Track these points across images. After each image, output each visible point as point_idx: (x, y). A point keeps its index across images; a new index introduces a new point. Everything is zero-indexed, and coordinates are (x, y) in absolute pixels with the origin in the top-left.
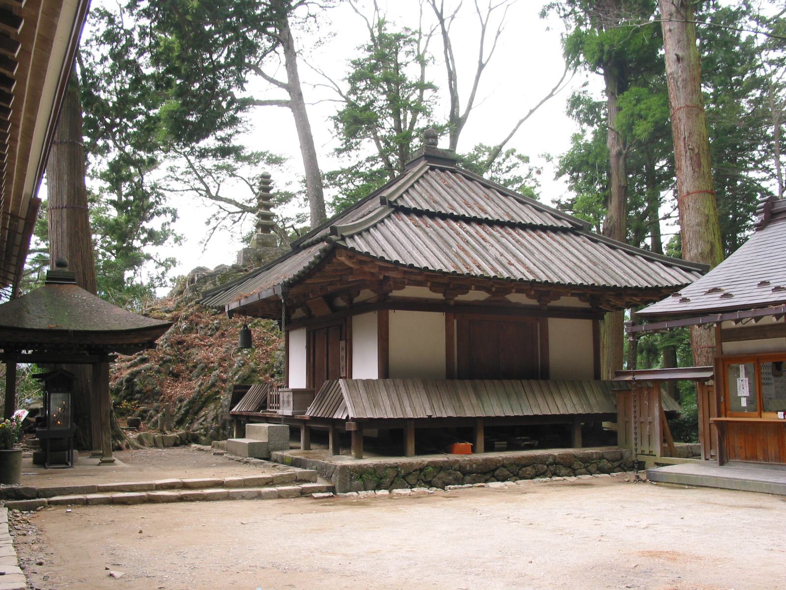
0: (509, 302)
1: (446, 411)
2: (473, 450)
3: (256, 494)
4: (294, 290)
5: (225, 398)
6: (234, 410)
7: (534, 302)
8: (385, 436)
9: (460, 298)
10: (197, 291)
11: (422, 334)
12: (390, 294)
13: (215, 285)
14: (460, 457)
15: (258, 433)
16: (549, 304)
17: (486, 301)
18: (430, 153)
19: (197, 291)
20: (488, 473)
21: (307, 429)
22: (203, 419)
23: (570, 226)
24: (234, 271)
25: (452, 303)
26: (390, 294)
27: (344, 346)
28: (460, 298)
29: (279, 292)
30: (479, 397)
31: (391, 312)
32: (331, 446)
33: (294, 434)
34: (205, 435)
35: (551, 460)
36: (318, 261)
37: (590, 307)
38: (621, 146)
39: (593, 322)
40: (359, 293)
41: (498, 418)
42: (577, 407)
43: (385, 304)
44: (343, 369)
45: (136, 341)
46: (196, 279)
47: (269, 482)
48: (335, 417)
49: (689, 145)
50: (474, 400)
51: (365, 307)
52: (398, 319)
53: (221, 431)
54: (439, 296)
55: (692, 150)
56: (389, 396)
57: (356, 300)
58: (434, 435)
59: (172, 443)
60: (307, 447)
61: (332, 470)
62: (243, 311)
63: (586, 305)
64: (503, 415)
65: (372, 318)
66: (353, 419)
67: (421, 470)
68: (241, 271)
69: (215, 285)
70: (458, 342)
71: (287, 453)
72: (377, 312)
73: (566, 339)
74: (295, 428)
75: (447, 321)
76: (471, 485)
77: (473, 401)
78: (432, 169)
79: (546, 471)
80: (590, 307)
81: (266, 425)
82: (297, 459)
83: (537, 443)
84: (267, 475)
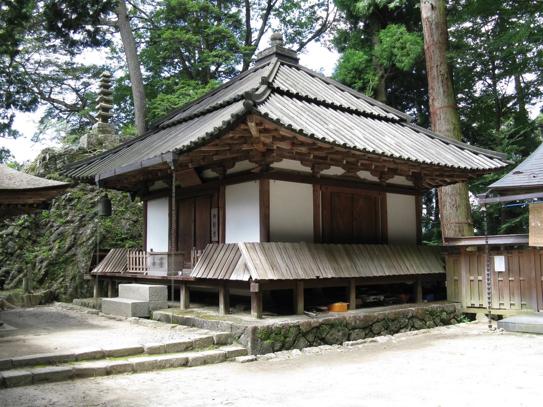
0: (359, 178)
1: (328, 272)
2: (349, 308)
3: (184, 362)
4: (182, 158)
5: (82, 260)
6: (95, 270)
7: (375, 179)
8: (276, 297)
9: (325, 172)
10: (48, 168)
11: (295, 202)
12: (271, 165)
13: (64, 163)
14: (339, 312)
15: (133, 294)
16: (387, 181)
17: (343, 175)
18: (279, 52)
19: (48, 168)
20: (369, 329)
21: (187, 289)
22: (61, 279)
23: (397, 118)
24: (81, 152)
25: (319, 176)
26: (271, 165)
27: (216, 213)
28: (325, 172)
29: (169, 159)
30: (351, 259)
31: (272, 182)
32: (222, 306)
33: (173, 296)
34: (65, 294)
35: (410, 314)
36: (224, 127)
37: (413, 185)
38: (383, 71)
39: (416, 198)
40: (234, 165)
41: (375, 277)
42: (385, 269)
43: (265, 174)
44: (215, 233)
45: (31, 201)
46: (48, 157)
47: (189, 347)
48: (233, 277)
49: (441, 71)
50: (349, 264)
51: (245, 177)
52: (278, 189)
53: (79, 290)
54: (308, 170)
55: (443, 75)
56: (283, 258)
57: (230, 171)
58: (320, 294)
59: (38, 301)
60: (186, 307)
61: (240, 331)
62: (106, 184)
63: (410, 183)
64: (371, 276)
65: (253, 187)
66: (257, 281)
67: (318, 328)
68: (87, 152)
69: (64, 163)
70: (322, 211)
71: (169, 313)
72: (258, 181)
73: (399, 210)
74: (173, 289)
75: (314, 191)
76: (363, 341)
77: (348, 264)
78: (282, 64)
79: (407, 324)
80: (413, 185)
81: (148, 286)
82: (187, 318)
83: (382, 298)
84: (185, 339)
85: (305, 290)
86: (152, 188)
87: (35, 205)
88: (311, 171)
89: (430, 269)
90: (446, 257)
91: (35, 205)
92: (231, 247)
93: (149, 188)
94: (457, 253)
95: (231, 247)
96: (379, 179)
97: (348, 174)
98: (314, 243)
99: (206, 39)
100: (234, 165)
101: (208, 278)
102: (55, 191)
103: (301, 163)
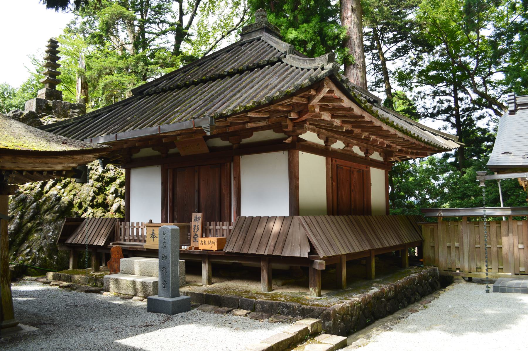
26: (300, 136)
48: (287, 253)
54: (321, 142)
57: (245, 141)
85: (347, 262)
86: (136, 156)
87: (64, 173)
88: (324, 144)
89: (369, 240)
90: (423, 227)
91: (64, 173)
92: (108, 221)
93: (132, 155)
94: (434, 223)
95: (108, 221)
96: (365, 154)
97: (346, 148)
98: (328, 214)
99: (95, 7)
100: (252, 135)
101: (266, 254)
102: (91, 156)
103: (318, 135)
